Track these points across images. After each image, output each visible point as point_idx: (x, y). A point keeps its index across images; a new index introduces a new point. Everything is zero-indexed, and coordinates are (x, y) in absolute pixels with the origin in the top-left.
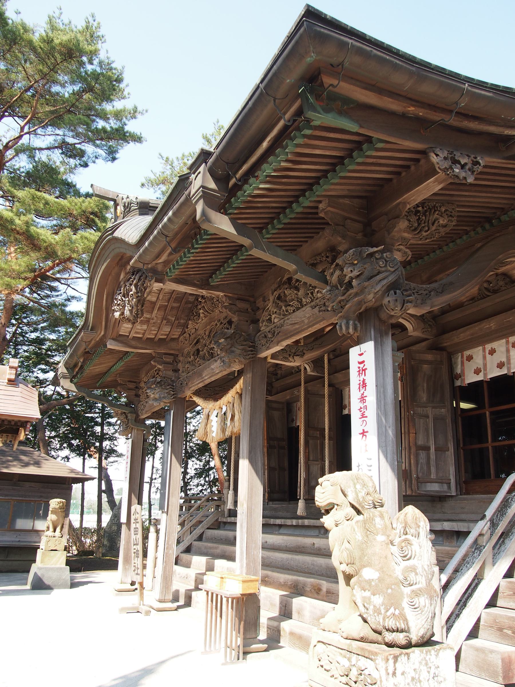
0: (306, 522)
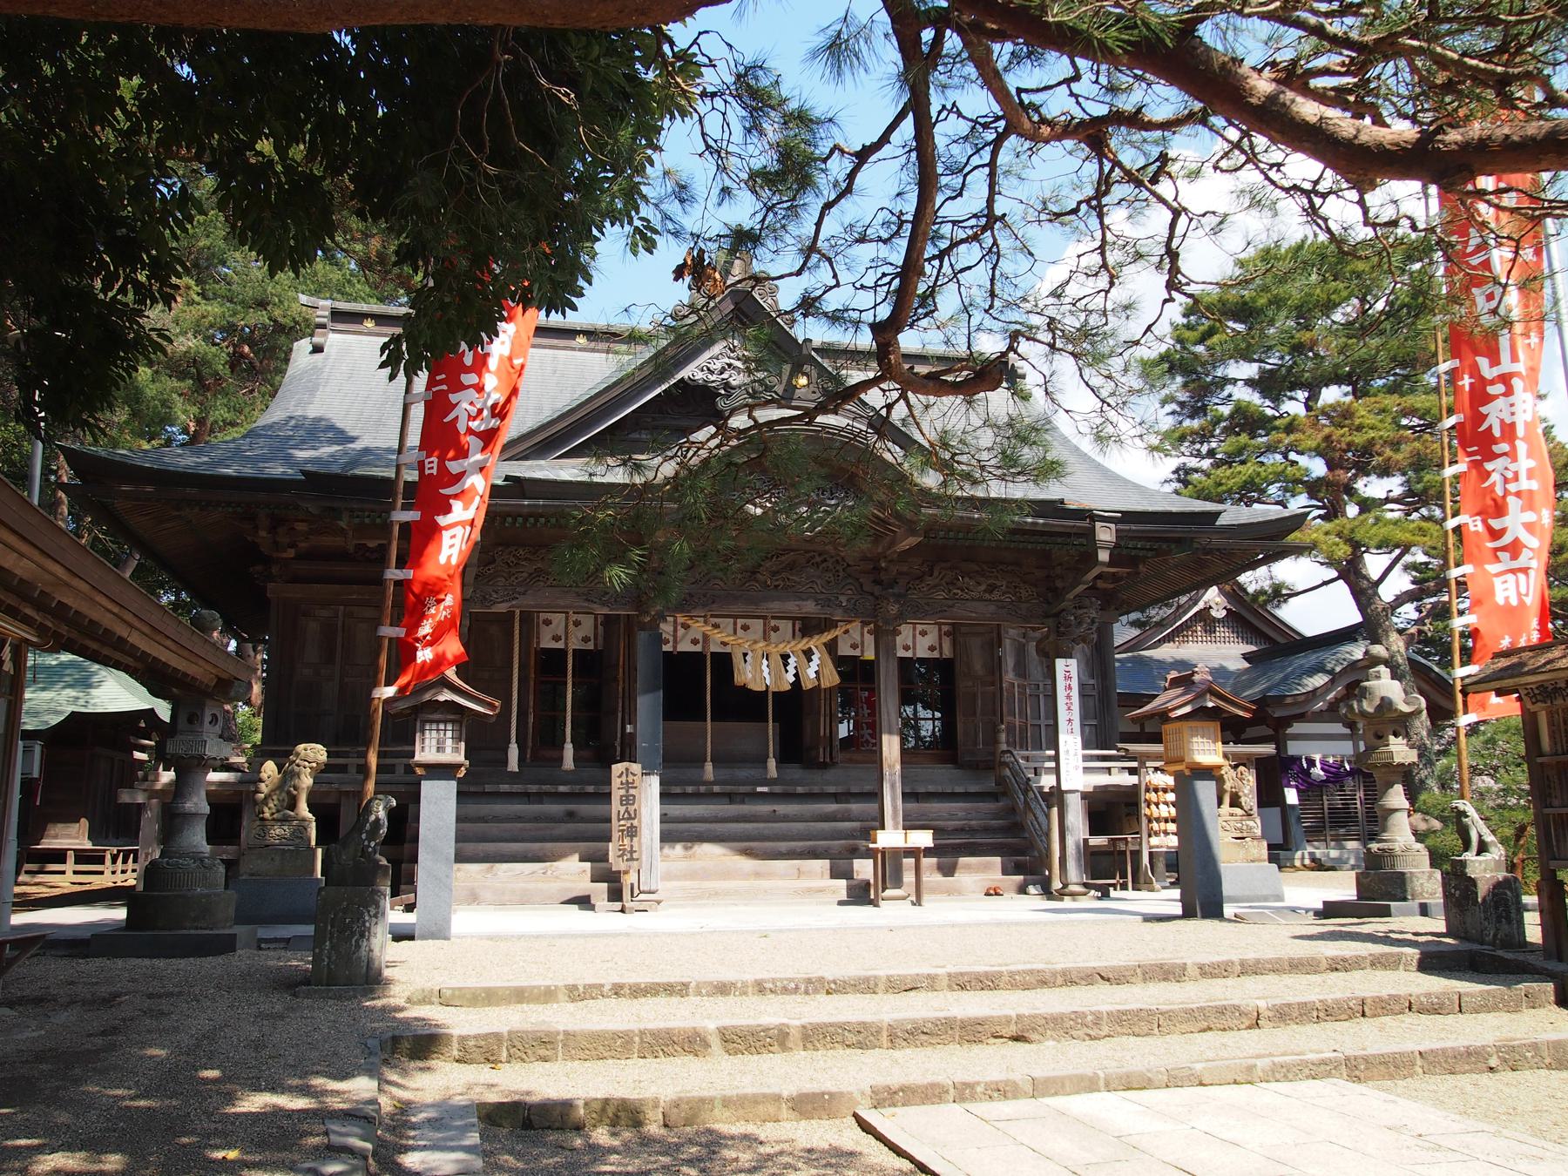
0: (716, 789)
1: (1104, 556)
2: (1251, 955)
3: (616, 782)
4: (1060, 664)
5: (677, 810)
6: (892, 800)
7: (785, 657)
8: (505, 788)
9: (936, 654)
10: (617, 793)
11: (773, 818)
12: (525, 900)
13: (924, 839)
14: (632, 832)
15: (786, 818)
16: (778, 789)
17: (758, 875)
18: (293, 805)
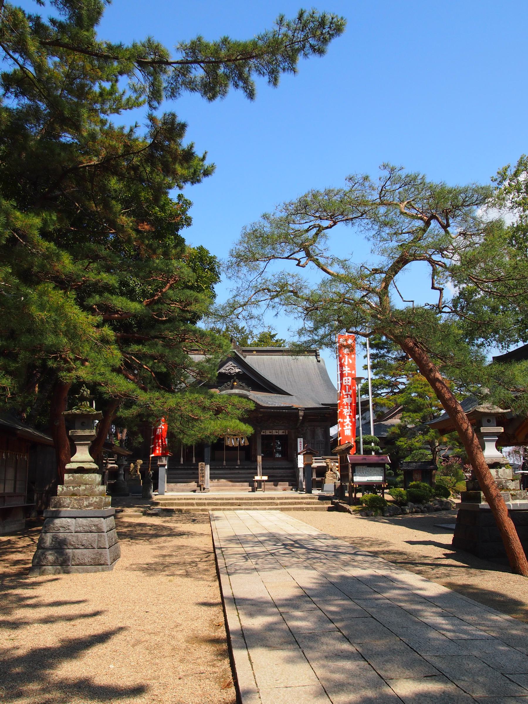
1: (301, 418)
2: (287, 496)
3: (200, 466)
4: (299, 439)
5: (213, 472)
6: (259, 470)
7: (237, 439)
8: (180, 467)
9: (284, 434)
10: (200, 469)
11: (239, 473)
12: (183, 491)
13: (265, 478)
14: (203, 477)
15: (241, 474)
16: (241, 467)
17: (233, 486)
18: (137, 472)
